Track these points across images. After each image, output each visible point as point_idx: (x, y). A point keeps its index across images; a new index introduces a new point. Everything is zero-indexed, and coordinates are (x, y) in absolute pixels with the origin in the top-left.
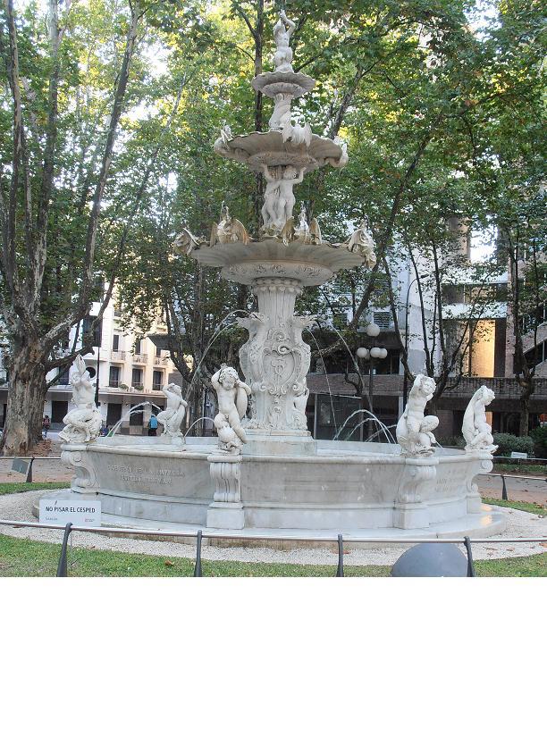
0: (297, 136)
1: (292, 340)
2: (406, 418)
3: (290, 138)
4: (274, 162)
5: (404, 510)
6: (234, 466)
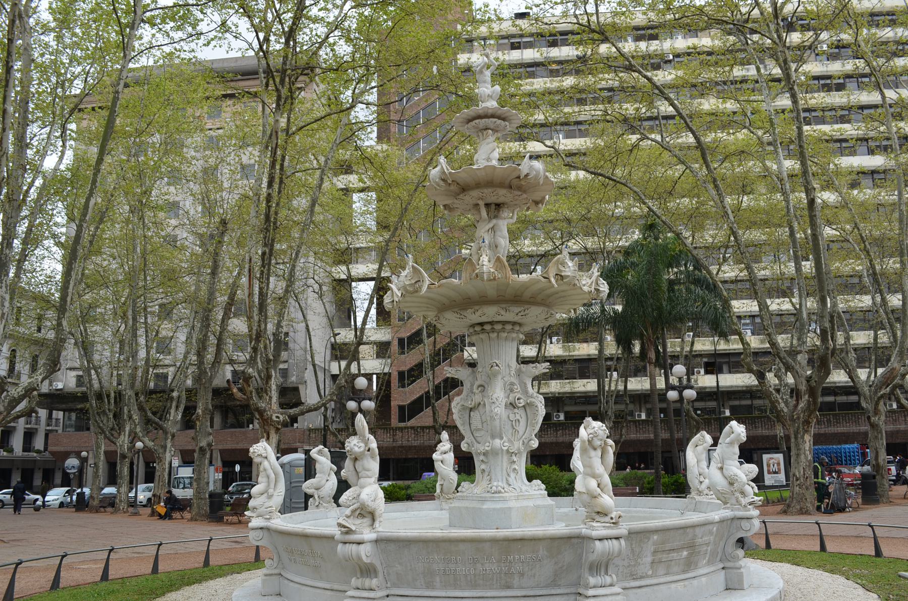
0: (538, 172)
1: (526, 392)
2: (721, 469)
3: (527, 175)
4: (493, 199)
5: (739, 568)
6: (623, 541)
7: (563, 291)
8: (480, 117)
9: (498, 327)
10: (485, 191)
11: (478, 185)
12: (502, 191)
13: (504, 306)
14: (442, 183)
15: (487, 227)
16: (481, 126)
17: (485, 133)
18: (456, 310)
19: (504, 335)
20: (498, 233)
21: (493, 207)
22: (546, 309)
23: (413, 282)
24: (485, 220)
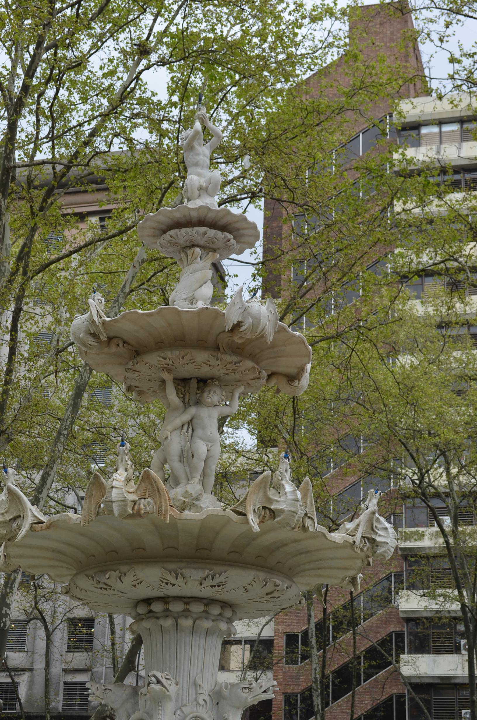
0: (257, 319)
3: (239, 324)
4: (188, 370)
7: (295, 541)
8: (189, 223)
9: (177, 607)
10: (169, 354)
11: (160, 344)
12: (202, 356)
13: (172, 566)
14: (90, 340)
15: (178, 422)
16: (182, 241)
17: (189, 252)
18: (91, 572)
19: (186, 623)
20: (199, 432)
21: (194, 384)
22: (262, 575)
23: (8, 517)
24: (176, 409)
